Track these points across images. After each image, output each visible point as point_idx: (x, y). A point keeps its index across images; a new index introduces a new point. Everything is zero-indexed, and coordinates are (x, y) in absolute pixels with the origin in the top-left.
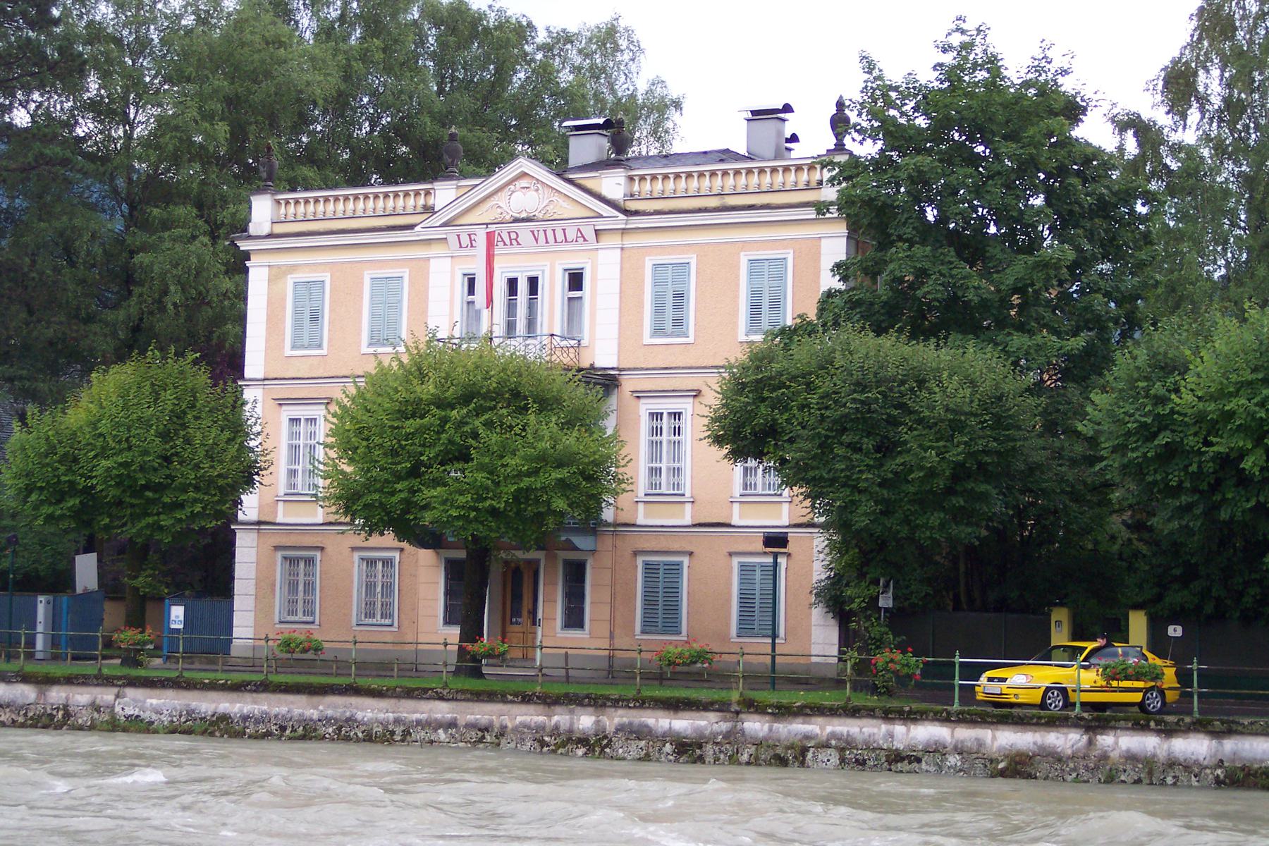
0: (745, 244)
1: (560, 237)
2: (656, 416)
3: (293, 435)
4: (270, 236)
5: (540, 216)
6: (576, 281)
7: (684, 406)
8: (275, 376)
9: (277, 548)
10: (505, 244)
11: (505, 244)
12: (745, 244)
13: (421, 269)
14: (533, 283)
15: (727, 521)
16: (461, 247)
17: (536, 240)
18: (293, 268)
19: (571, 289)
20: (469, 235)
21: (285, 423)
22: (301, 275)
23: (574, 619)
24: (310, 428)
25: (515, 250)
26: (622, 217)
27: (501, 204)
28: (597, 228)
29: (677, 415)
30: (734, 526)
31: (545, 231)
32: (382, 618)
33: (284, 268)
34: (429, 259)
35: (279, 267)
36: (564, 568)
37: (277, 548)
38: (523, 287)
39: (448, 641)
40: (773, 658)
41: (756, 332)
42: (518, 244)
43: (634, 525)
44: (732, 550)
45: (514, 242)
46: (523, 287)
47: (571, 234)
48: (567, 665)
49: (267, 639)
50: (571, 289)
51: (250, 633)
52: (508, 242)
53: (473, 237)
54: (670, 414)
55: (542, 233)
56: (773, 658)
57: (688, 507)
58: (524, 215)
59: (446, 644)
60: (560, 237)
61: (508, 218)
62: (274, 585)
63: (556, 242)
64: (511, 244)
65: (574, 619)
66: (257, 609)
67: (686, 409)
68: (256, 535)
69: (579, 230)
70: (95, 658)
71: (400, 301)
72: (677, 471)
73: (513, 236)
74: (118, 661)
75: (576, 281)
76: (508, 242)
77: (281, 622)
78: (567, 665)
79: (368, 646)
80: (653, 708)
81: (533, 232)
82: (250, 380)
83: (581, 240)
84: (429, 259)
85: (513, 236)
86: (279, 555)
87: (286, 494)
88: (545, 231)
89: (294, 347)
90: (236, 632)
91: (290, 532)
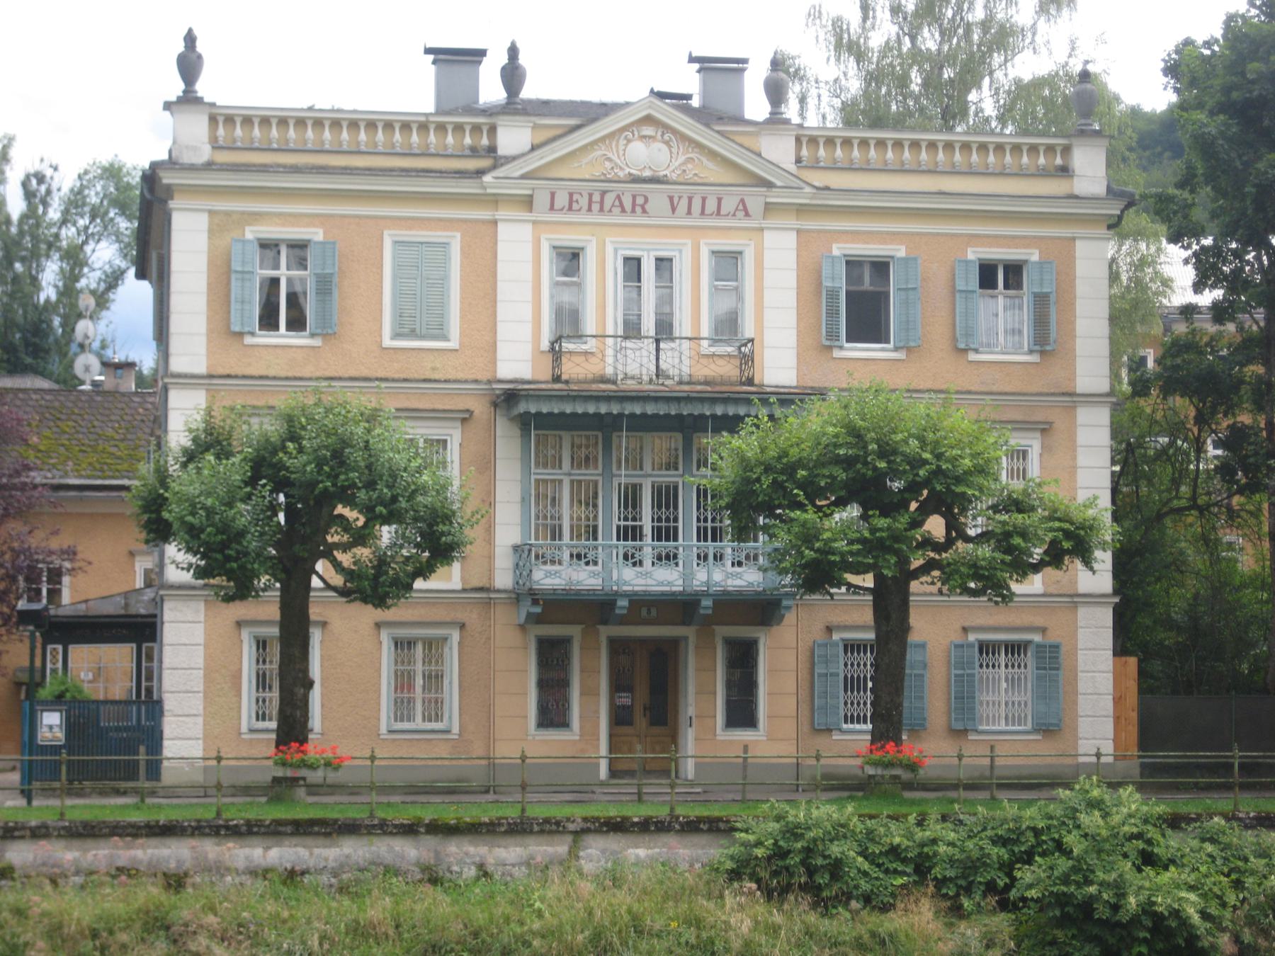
0: (974, 239)
1: (711, 206)
4: (209, 166)
5: (674, 177)
7: (450, 431)
8: (227, 372)
9: (239, 624)
10: (623, 211)
11: (623, 211)
12: (974, 239)
14: (663, 264)
17: (674, 209)
18: (256, 217)
20: (571, 195)
22: (303, 230)
26: (808, 190)
27: (610, 155)
28: (769, 200)
31: (690, 199)
32: (424, 720)
34: (1074, 239)
35: (228, 214)
37: (239, 624)
38: (648, 269)
41: (727, 342)
42: (644, 211)
44: (967, 624)
45: (638, 209)
47: (729, 204)
48: (745, 777)
49: (219, 759)
51: (195, 749)
52: (628, 206)
53: (575, 197)
56: (992, 758)
58: (647, 173)
59: (219, 759)
60: (711, 206)
62: (237, 676)
63: (703, 213)
64: (633, 211)
66: (209, 715)
68: (202, 605)
69: (742, 201)
70: (1228, 787)
71: (445, 278)
74: (264, 799)
76: (628, 206)
77: (390, 732)
78: (745, 777)
79: (765, 761)
81: (671, 198)
82: (179, 376)
83: (741, 214)
84: (1074, 239)
85: (640, 201)
88: (690, 199)
89: (396, 336)
90: (171, 748)
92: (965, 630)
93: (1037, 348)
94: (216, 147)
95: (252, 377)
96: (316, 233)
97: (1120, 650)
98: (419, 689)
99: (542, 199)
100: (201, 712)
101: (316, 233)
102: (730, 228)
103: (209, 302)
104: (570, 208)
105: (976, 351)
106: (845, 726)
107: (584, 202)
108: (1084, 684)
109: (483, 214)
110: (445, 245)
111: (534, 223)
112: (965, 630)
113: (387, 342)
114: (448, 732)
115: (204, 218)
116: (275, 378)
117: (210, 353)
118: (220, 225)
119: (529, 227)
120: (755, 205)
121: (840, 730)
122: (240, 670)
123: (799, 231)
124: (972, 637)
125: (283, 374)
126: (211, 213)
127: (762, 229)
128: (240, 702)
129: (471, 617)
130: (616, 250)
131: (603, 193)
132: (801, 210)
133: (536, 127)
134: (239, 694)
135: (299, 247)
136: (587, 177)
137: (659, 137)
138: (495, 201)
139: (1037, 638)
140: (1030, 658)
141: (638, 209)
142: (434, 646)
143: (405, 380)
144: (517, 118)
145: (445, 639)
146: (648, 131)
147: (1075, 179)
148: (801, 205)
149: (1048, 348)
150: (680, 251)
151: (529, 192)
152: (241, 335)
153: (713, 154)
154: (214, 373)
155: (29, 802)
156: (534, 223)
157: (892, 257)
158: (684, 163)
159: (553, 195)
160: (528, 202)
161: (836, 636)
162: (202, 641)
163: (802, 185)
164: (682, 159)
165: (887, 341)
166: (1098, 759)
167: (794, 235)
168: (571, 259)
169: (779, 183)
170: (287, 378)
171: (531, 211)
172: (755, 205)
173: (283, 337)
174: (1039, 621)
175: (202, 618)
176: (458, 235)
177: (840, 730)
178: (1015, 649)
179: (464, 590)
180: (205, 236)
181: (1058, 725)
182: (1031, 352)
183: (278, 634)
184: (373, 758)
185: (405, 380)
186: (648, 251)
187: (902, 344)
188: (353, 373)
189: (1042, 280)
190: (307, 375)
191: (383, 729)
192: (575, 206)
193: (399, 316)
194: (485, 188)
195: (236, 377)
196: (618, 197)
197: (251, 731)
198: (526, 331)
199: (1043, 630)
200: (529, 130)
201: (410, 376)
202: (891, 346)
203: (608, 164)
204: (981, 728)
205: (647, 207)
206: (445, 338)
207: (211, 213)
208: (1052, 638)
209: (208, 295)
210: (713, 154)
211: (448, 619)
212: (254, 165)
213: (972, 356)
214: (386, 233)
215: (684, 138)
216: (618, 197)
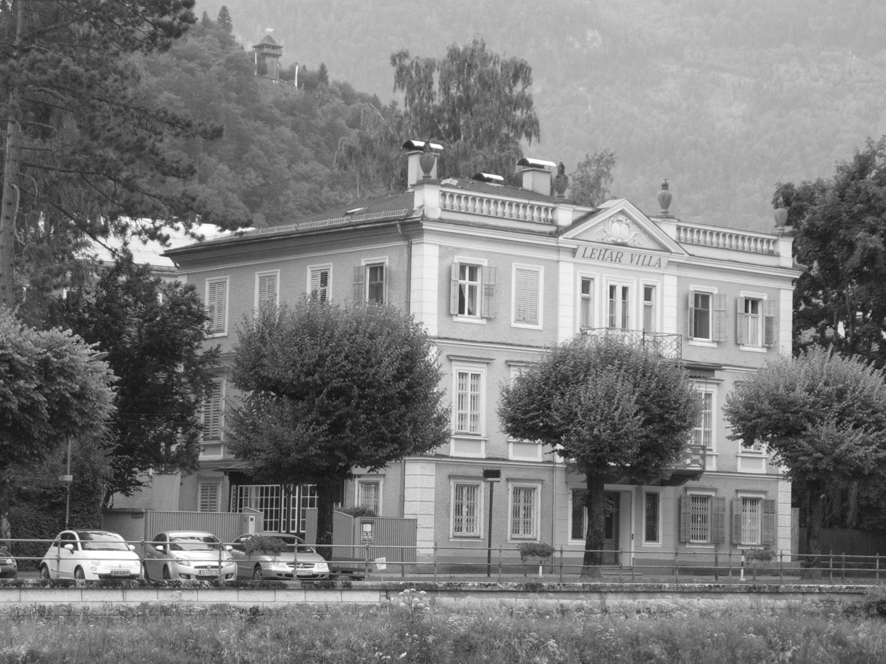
2: (462, 375)
3: (461, 386)
5: (630, 244)
6: (648, 293)
9: (450, 477)
10: (612, 260)
11: (612, 260)
13: (553, 269)
14: (625, 290)
15: (504, 457)
16: (583, 256)
18: (459, 250)
19: (583, 292)
20: (593, 250)
21: (455, 376)
23: (652, 535)
24: (475, 382)
25: (617, 266)
26: (687, 255)
29: (476, 376)
30: (511, 461)
33: (450, 249)
34: (780, 289)
35: (447, 248)
36: (647, 498)
37: (450, 477)
38: (619, 292)
39: (564, 549)
40: (489, 551)
42: (620, 261)
43: (737, 473)
44: (737, 489)
45: (618, 260)
46: (619, 292)
50: (583, 292)
54: (472, 374)
55: (637, 257)
56: (489, 551)
57: (483, 444)
58: (619, 241)
61: (610, 240)
65: (652, 535)
66: (437, 528)
67: (457, 370)
68: (434, 466)
70: (872, 575)
72: (475, 418)
73: (620, 255)
75: (648, 293)
77: (512, 539)
80: (62, 589)
81: (632, 255)
84: (780, 289)
85: (620, 255)
86: (452, 483)
87: (456, 434)
89: (517, 321)
91: (460, 465)
92: (737, 491)
93: (767, 345)
94: (444, 210)
95: (456, 340)
96: (484, 261)
97: (794, 505)
98: (521, 516)
99: (580, 252)
100: (433, 526)
101: (484, 261)
102: (651, 273)
103: (439, 296)
104: (590, 258)
105: (743, 345)
106: (691, 541)
107: (597, 254)
108: (780, 523)
109: (553, 256)
110: (537, 272)
111: (575, 263)
112: (737, 491)
113: (514, 325)
114: (535, 539)
115: (437, 248)
116: (466, 341)
117: (439, 325)
118: (445, 253)
119: (572, 265)
120: (664, 262)
121: (690, 543)
122: (450, 503)
123: (678, 277)
124: (740, 495)
125: (469, 339)
126: (440, 246)
127: (664, 274)
128: (449, 521)
129: (545, 476)
130: (607, 281)
131: (606, 250)
132: (680, 265)
133: (574, 211)
134: (449, 517)
135: (473, 270)
136: (595, 240)
137: (624, 221)
138: (558, 249)
139: (763, 496)
140: (759, 507)
141: (618, 260)
142: (530, 491)
143: (520, 346)
144: (568, 205)
145: (534, 489)
146: (621, 217)
147: (781, 258)
148: (680, 263)
149: (772, 346)
150: (632, 283)
151: (575, 247)
152: (452, 315)
153: (645, 232)
154: (441, 336)
155: (489, 575)
156: (575, 263)
157: (712, 293)
158: (634, 236)
159: (586, 249)
160: (574, 252)
161: (689, 493)
162: (433, 486)
163: (684, 253)
164: (633, 234)
165: (707, 337)
166: (220, 563)
167: (676, 278)
168: (586, 285)
169: (673, 251)
170: (471, 341)
171: (574, 257)
172: (664, 262)
173: (465, 318)
174: (764, 488)
175: (434, 473)
176: (543, 267)
177: (690, 543)
178: (754, 501)
179: (543, 462)
180: (437, 259)
181: (773, 542)
182: (763, 347)
183: (586, 487)
184: (730, 555)
185: (520, 346)
186: (620, 282)
187: (716, 340)
188: (499, 341)
189: (769, 310)
190: (479, 340)
191: (509, 538)
192: (593, 256)
193: (518, 310)
194: (558, 243)
195: (449, 339)
196: (612, 253)
197: (455, 537)
198: (570, 322)
199: (765, 492)
200: (571, 212)
201: (522, 344)
202: (710, 339)
203: (604, 235)
204: (743, 543)
205: (621, 259)
206: (537, 324)
207: (440, 246)
208: (770, 497)
209: (439, 292)
210: (645, 232)
211: (535, 478)
212: (500, 227)
213: (742, 348)
214: (514, 264)
215: (635, 222)
216: (612, 253)
